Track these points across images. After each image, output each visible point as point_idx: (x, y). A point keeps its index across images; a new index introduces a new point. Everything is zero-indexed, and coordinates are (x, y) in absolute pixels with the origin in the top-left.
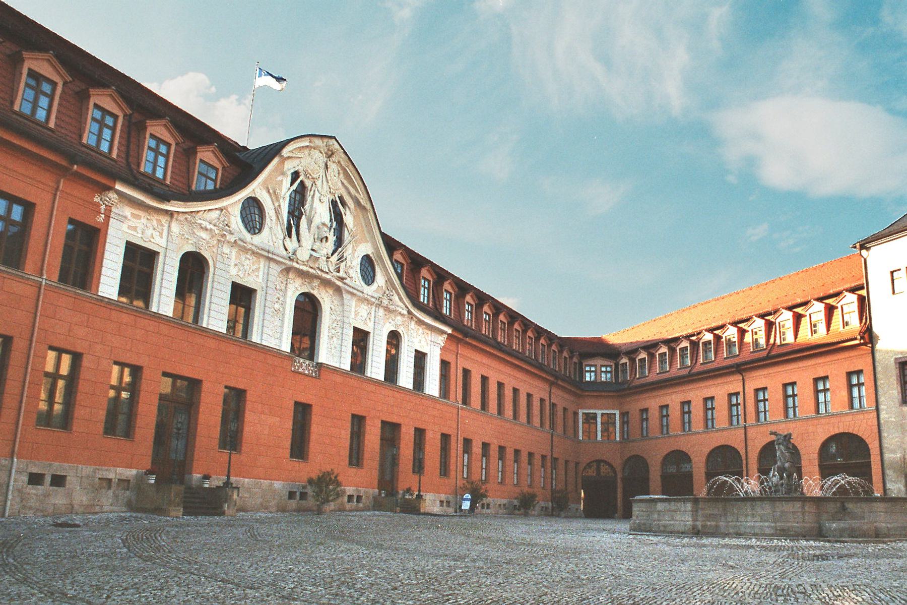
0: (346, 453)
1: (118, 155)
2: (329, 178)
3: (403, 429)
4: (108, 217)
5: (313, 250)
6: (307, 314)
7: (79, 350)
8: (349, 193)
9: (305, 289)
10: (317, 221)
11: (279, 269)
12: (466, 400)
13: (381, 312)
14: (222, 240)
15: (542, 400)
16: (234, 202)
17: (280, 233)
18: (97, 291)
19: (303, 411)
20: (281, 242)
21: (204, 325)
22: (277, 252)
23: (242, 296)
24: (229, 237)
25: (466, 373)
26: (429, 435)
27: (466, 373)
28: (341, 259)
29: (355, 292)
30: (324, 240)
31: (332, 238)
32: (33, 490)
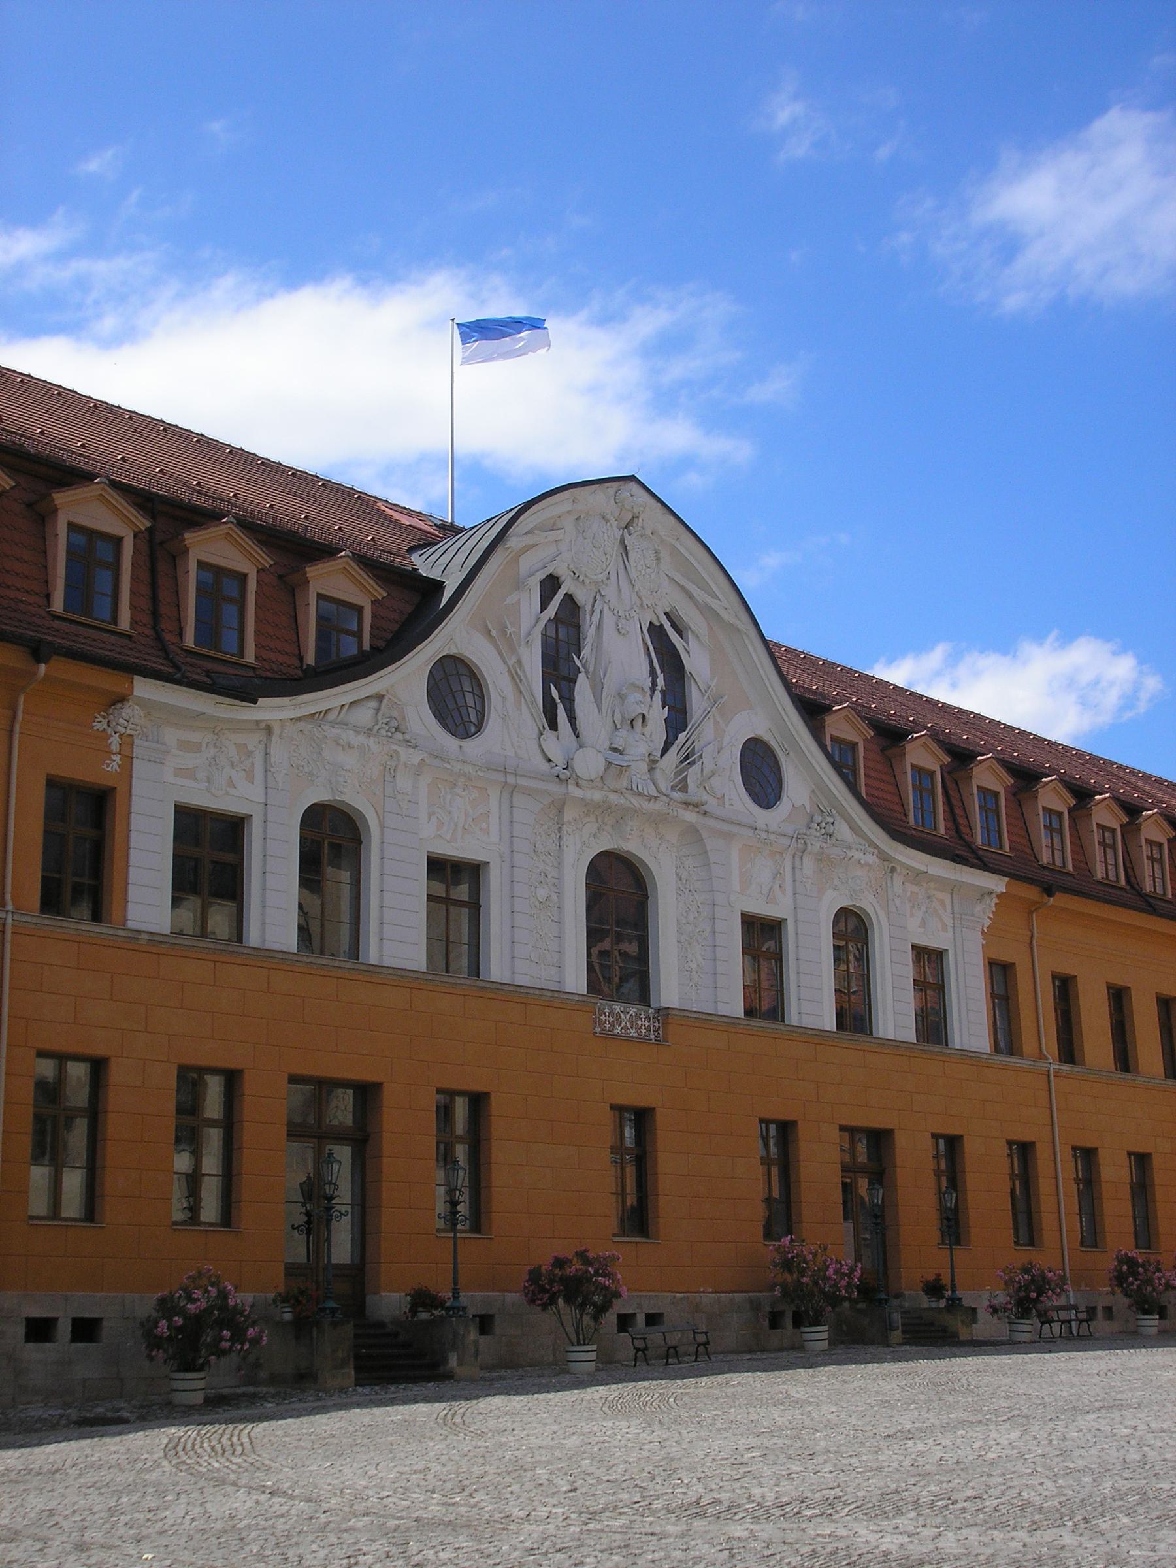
1: (134, 623)
2: (633, 574)
4: (128, 760)
5: (615, 750)
6: (619, 900)
7: (99, 1051)
10: (612, 682)
12: (1069, 1051)
16: (407, 678)
17: (530, 718)
18: (125, 920)
21: (373, 960)
23: (455, 881)
25: (1065, 987)
26: (972, 1148)
27: (1065, 987)
28: (688, 759)
31: (658, 714)
32: (34, 1352)
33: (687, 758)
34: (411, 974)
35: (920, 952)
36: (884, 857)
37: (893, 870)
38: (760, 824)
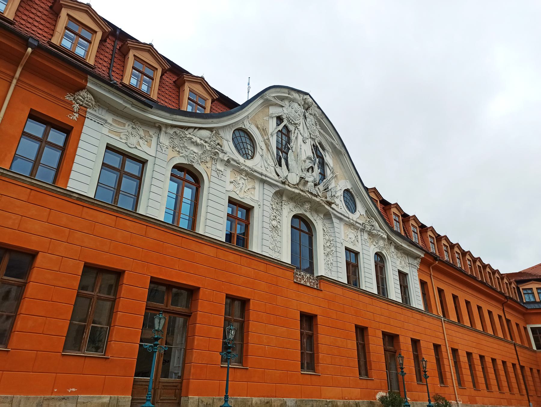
0: (355, 363)
2: (308, 125)
3: (401, 339)
8: (327, 140)
9: (298, 211)
11: (274, 191)
13: (366, 236)
14: (214, 156)
15: (514, 365)
19: (308, 319)
20: (273, 169)
22: (268, 174)
24: (221, 155)
29: (342, 217)
30: (310, 170)
33: (325, 190)
34: (206, 238)
35: (400, 272)
36: (211, 129)
37: (391, 243)
38: (350, 217)
